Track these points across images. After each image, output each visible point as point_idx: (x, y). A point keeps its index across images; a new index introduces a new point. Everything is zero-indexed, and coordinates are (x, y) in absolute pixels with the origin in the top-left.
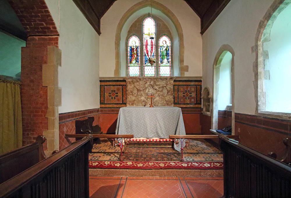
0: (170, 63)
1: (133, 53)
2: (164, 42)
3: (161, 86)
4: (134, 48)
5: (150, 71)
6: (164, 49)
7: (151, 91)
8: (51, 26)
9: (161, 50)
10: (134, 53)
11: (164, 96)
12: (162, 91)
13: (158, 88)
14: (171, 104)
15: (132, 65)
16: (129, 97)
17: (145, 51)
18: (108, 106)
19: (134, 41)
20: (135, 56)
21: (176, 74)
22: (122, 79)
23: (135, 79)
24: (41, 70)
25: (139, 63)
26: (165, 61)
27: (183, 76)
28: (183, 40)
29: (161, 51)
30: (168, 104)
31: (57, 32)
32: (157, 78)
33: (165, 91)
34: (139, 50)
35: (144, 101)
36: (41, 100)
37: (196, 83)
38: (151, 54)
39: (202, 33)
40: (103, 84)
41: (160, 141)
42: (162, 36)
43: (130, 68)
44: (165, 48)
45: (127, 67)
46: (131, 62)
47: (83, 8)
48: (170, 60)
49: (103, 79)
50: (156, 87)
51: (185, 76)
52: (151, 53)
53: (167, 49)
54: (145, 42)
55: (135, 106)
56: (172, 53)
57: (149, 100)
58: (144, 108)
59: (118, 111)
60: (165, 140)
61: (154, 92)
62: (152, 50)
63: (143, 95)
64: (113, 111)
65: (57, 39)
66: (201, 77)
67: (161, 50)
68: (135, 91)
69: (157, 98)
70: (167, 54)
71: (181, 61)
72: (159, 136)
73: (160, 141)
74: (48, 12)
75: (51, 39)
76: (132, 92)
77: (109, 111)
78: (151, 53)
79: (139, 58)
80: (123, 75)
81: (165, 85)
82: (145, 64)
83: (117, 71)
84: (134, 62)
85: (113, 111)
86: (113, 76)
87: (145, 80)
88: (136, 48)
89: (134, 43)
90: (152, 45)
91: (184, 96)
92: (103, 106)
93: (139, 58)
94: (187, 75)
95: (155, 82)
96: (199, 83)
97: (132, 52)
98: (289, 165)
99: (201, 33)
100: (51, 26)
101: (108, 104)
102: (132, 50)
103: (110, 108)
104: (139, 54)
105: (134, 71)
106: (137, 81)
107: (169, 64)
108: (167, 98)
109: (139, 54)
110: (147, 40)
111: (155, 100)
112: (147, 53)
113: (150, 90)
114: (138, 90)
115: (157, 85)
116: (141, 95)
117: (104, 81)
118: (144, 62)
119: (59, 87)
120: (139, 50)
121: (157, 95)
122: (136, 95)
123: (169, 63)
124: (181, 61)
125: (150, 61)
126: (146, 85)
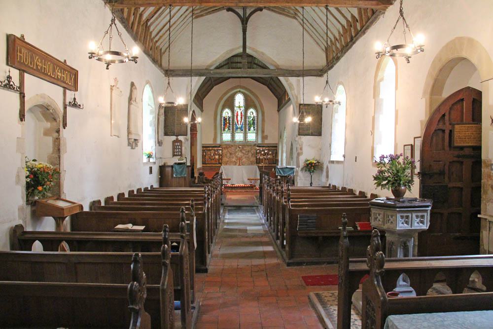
0: (256, 130)
2: (251, 113)
5: (239, 137)
6: (251, 119)
7: (240, 154)
12: (247, 154)
15: (225, 132)
17: (236, 121)
18: (208, 165)
19: (227, 113)
21: (260, 142)
25: (231, 130)
26: (252, 128)
30: (252, 163)
32: (245, 144)
33: (250, 154)
35: (235, 162)
37: (273, 148)
39: (278, 111)
45: (221, 134)
46: (224, 130)
48: (256, 128)
50: (244, 152)
56: (257, 123)
57: (238, 161)
58: (234, 166)
62: (241, 120)
66: (277, 144)
68: (228, 155)
70: (254, 123)
71: (263, 132)
72: (244, 183)
76: (226, 155)
79: (231, 126)
80: (218, 142)
83: (215, 139)
84: (227, 130)
90: (242, 116)
92: (205, 165)
93: (231, 126)
94: (266, 142)
102: (225, 119)
104: (231, 123)
105: (227, 137)
106: (230, 147)
107: (255, 132)
108: (252, 159)
109: (231, 123)
112: (238, 123)
114: (230, 154)
116: (233, 158)
117: (205, 147)
119: (483, 157)
124: (263, 132)
125: (241, 128)
126: (237, 150)
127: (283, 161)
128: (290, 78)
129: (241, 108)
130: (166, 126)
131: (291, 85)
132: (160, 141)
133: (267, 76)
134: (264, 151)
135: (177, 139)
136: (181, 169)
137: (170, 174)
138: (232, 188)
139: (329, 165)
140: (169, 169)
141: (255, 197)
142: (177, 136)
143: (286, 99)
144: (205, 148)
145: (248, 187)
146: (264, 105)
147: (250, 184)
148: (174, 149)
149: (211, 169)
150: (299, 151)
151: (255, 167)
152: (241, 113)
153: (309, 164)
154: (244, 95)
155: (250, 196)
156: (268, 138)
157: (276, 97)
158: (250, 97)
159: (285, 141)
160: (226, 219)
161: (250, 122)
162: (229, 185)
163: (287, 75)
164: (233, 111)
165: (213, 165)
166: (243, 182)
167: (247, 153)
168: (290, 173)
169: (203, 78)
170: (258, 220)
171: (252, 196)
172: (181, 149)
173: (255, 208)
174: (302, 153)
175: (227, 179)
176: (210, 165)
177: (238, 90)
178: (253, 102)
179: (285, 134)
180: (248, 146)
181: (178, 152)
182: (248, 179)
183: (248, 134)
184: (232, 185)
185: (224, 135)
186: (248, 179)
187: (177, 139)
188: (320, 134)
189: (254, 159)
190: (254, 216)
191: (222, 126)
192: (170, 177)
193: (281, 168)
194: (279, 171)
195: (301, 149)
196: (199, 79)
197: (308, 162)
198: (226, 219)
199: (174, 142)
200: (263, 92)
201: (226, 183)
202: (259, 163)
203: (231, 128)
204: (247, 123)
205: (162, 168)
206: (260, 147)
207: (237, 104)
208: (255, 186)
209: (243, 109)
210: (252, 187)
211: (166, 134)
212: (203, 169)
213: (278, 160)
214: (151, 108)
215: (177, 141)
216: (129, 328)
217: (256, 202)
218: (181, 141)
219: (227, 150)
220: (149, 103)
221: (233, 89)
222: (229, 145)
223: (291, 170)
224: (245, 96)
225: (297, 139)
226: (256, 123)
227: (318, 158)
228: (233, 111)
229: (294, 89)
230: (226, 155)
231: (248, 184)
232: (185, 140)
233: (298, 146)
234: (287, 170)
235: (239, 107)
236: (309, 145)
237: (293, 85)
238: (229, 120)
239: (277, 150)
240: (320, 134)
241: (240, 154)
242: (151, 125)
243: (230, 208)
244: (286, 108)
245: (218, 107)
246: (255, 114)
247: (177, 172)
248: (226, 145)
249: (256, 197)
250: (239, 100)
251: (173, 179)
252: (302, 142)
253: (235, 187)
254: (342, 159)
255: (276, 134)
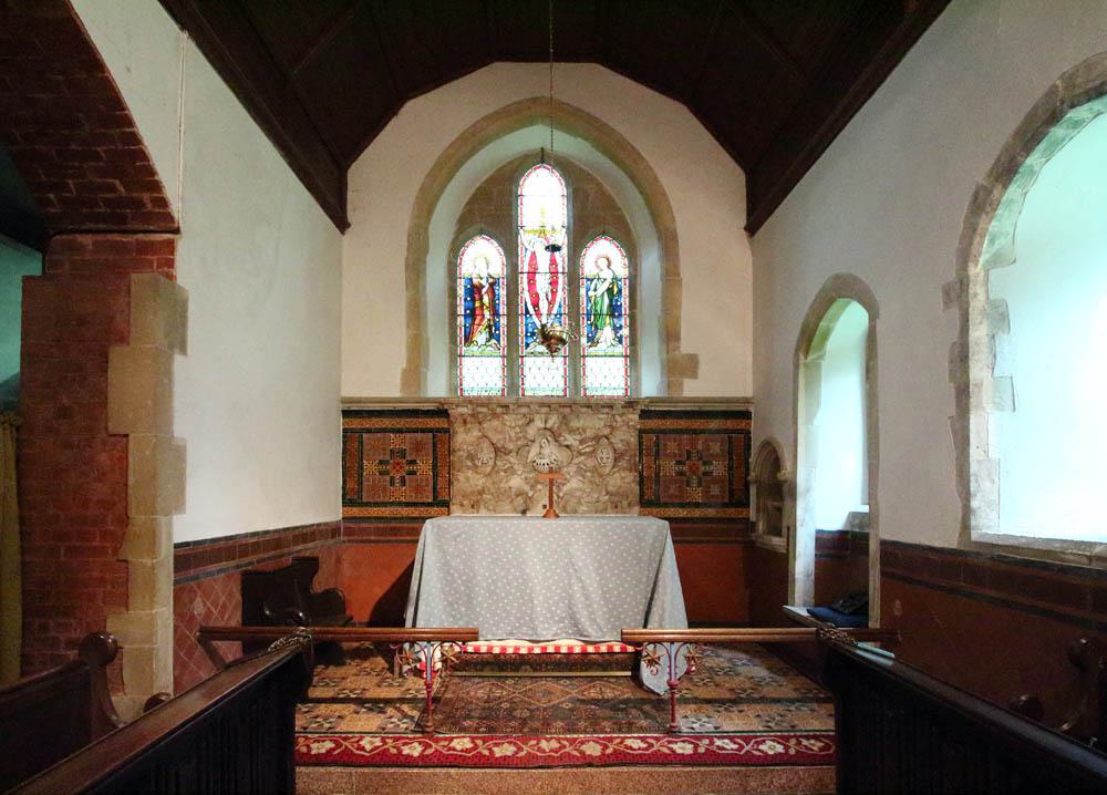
0: (626, 342)
2: (603, 263)
5: (544, 376)
6: (603, 288)
7: (549, 454)
15: (474, 348)
17: (526, 296)
18: (374, 512)
19: (482, 258)
25: (503, 342)
26: (607, 334)
32: (571, 406)
33: (606, 455)
39: (752, 228)
45: (455, 359)
46: (468, 339)
48: (625, 332)
50: (571, 440)
62: (554, 293)
68: (486, 455)
71: (670, 336)
72: (579, 632)
76: (471, 457)
79: (503, 321)
84: (481, 337)
90: (554, 273)
92: (355, 511)
102: (474, 290)
104: (503, 309)
105: (482, 374)
106: (495, 415)
107: (620, 349)
109: (503, 309)
112: (536, 305)
114: (497, 450)
116: (511, 471)
124: (670, 336)
126: (531, 431)
156: (703, 369)
164: (510, 248)
176: (386, 512)
185: (468, 365)
216: (1097, 776)
228: (510, 248)
245: (430, 211)
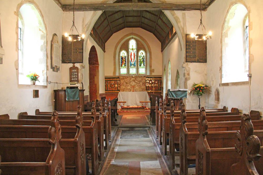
0: (145, 66)
1: (123, 60)
2: (142, 54)
3: (139, 81)
4: (124, 57)
5: (133, 71)
6: (142, 57)
7: (133, 83)
8: (97, 63)
9: (140, 58)
10: (123, 61)
11: (140, 86)
13: (137, 82)
14: (145, 90)
15: (122, 67)
16: (121, 87)
18: (109, 92)
19: (123, 53)
20: (124, 62)
21: (148, 74)
22: (117, 77)
23: (124, 77)
24: (94, 78)
25: (127, 66)
26: (142, 64)
27: (151, 75)
28: (151, 55)
29: (140, 59)
30: (143, 90)
31: (98, 64)
32: (138, 76)
33: (141, 83)
34: (126, 58)
35: (129, 89)
36: (94, 89)
38: (134, 61)
39: (162, 51)
40: (107, 79)
41: (137, 107)
42: (140, 50)
43: (121, 69)
44: (142, 57)
45: (119, 69)
46: (121, 66)
47: (98, 42)
48: (145, 64)
49: (107, 77)
51: (152, 75)
52: (134, 60)
53: (144, 58)
54: (130, 53)
55: (124, 91)
56: (146, 61)
58: (129, 93)
59: (118, 94)
60: (140, 107)
61: (136, 83)
62: (134, 59)
63: (129, 85)
64: (112, 94)
65: (98, 66)
66: (161, 76)
67: (140, 58)
68: (125, 84)
69: (137, 87)
70: (143, 61)
71: (151, 67)
73: (137, 107)
74: (98, 59)
75: (96, 67)
77: (110, 94)
78: (134, 60)
79: (127, 63)
80: (117, 75)
81: (141, 80)
82: (130, 67)
83: (115, 72)
84: (123, 66)
85: (112, 94)
86: (112, 75)
87: (130, 77)
88: (125, 58)
89: (123, 54)
90: (134, 55)
91: (115, 85)
92: (107, 92)
93: (127, 63)
94: (153, 74)
95: (135, 79)
96: (160, 79)
97: (122, 60)
98: (178, 110)
99: (161, 51)
100: (97, 63)
101: (110, 91)
102: (122, 58)
103: (111, 93)
104: (127, 61)
105: (123, 71)
106: (126, 78)
109: (127, 61)
110: (131, 53)
111: (136, 88)
112: (132, 60)
113: (133, 83)
115: (136, 80)
118: (129, 66)
120: (126, 58)
121: (137, 85)
122: (125, 86)
123: (144, 66)
124: (151, 67)
125: (134, 65)
126: (131, 80)
127: (168, 85)
128: (176, 12)
129: (134, 50)
130: (63, 54)
131: (177, 19)
132: (54, 66)
133: (156, 9)
134: (151, 80)
135: (74, 66)
136: (73, 93)
137: (63, 98)
138: (128, 108)
139: (221, 89)
140: (63, 93)
141: (146, 117)
142: (74, 63)
143: (170, 37)
144: (108, 79)
145: (140, 108)
146: (151, 47)
147: (142, 105)
148: (71, 75)
149: (112, 94)
150: (187, 76)
151: (146, 93)
152: (134, 54)
153: (197, 87)
154: (136, 40)
155: (141, 115)
157: (161, 42)
158: (140, 42)
159: (170, 71)
160: (117, 145)
161: (140, 60)
162: (125, 106)
163: (174, 8)
164: (128, 52)
165: (113, 92)
166: (136, 104)
167: (138, 83)
168: (182, 96)
169: (99, 13)
170: (150, 147)
171: (143, 115)
172: (78, 75)
173: (147, 129)
174: (189, 79)
175: (123, 102)
177: (131, 36)
178: (143, 45)
179: (170, 66)
180: (140, 77)
181: (75, 78)
182: (140, 102)
183: (140, 69)
184: (128, 106)
186: (140, 102)
187: (74, 66)
188: (205, 61)
189: (144, 87)
190: (146, 141)
191: (120, 63)
192: (63, 101)
193: (173, 91)
194: (172, 94)
195: (188, 74)
196: (94, 15)
197: (196, 86)
198: (117, 145)
199: (71, 69)
200: (150, 37)
201: (123, 105)
202: (148, 90)
203: (127, 65)
204: (139, 61)
205: (56, 93)
206: (148, 78)
207: (131, 47)
208: (146, 107)
209: (135, 50)
210: (143, 108)
211: (63, 62)
212: (106, 95)
213: (163, 88)
214: (42, 33)
215: (74, 68)
217: (147, 122)
218: (77, 68)
219: (123, 81)
220: (41, 28)
221: (127, 35)
222: (125, 77)
223: (183, 93)
224: (137, 41)
225: (184, 65)
226: (145, 61)
227: (204, 82)
228: (128, 52)
229: (180, 22)
230: (123, 84)
231: (140, 105)
232: (81, 67)
233: (186, 72)
234: (179, 93)
235: (133, 49)
236: (195, 71)
237: (178, 18)
238: (125, 59)
239: (161, 80)
240: (205, 61)
241: (133, 83)
242: (42, 50)
243: (123, 129)
244: (170, 44)
246: (144, 54)
247: (69, 96)
248: (122, 76)
249: (147, 116)
250: (133, 44)
251: (67, 103)
252: (189, 68)
253: (130, 108)
254: (247, 79)
255: (161, 69)
